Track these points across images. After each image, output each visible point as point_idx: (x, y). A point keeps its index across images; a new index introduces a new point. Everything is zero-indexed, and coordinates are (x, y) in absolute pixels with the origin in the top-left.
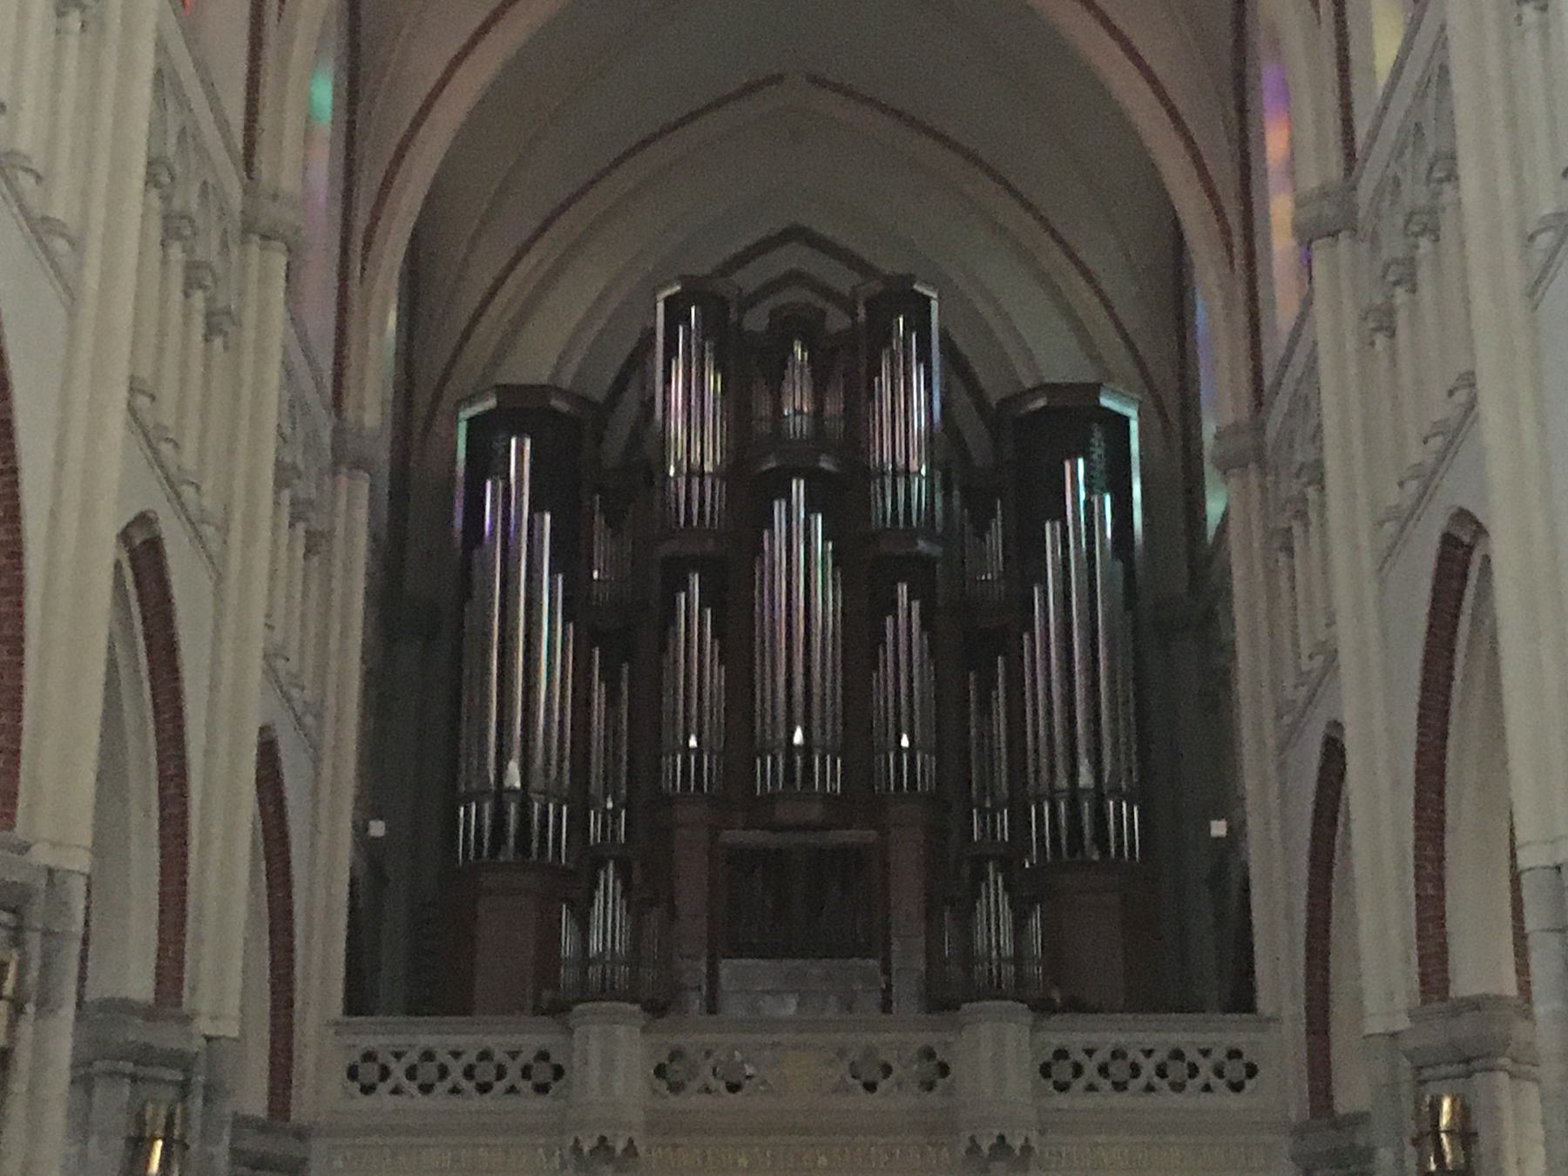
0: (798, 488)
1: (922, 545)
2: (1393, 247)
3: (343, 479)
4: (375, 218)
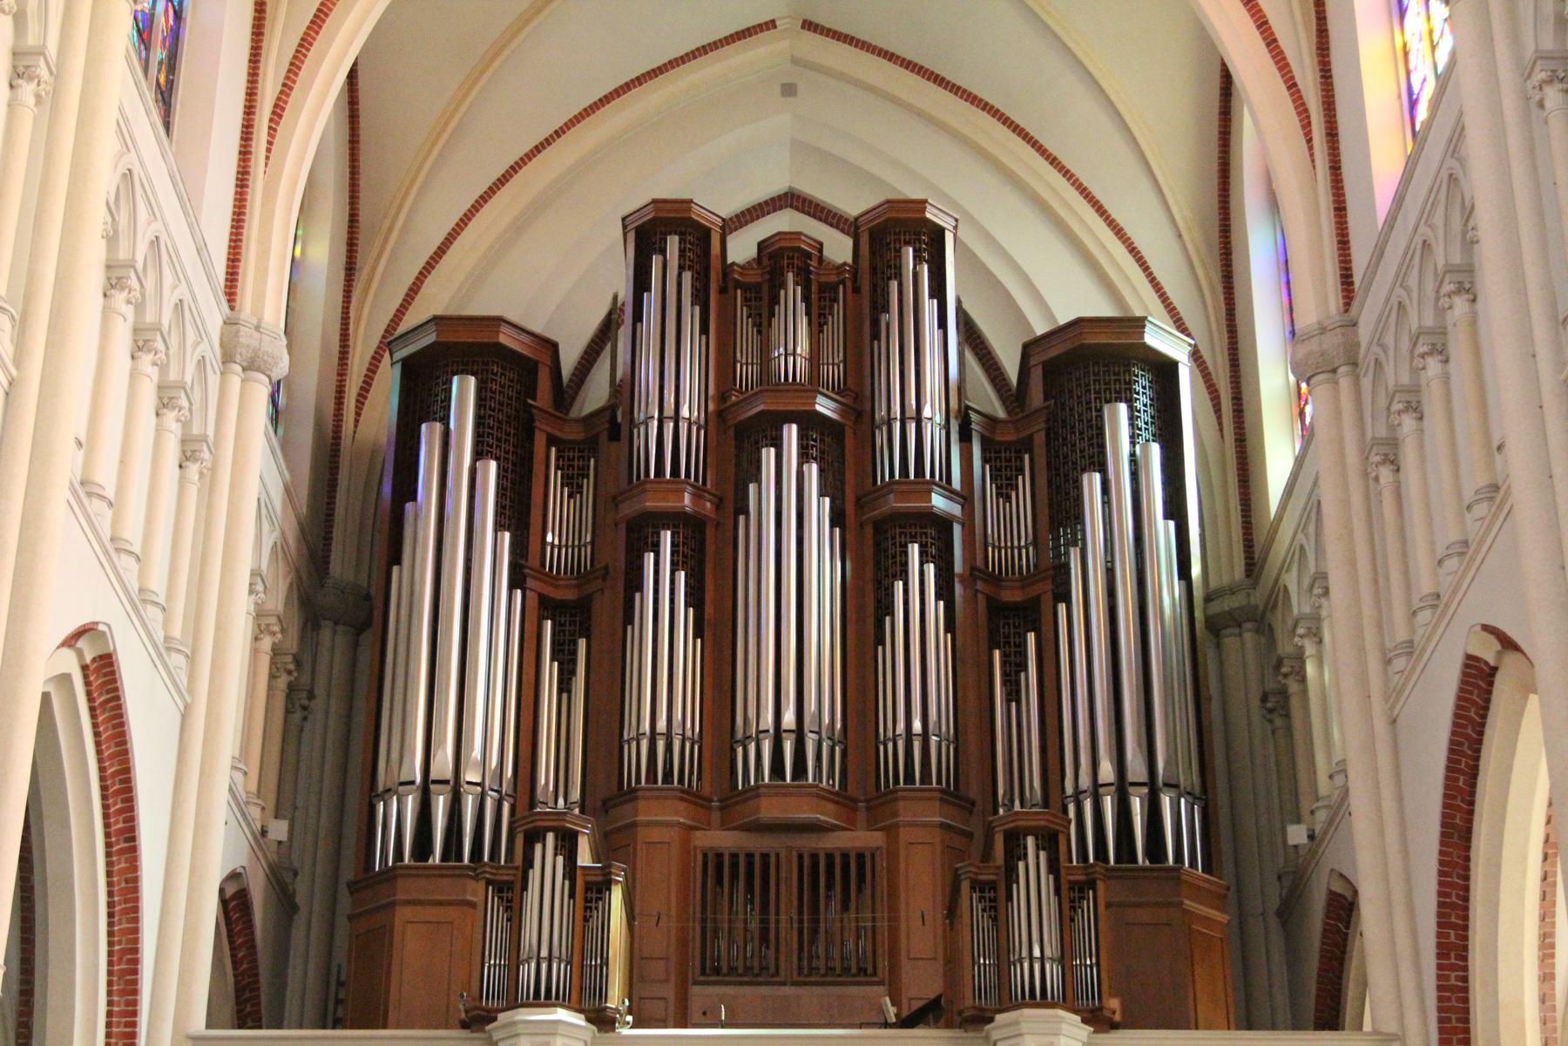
0: (791, 433)
1: (938, 501)
2: (1397, 374)
3: (235, 382)
4: (287, 88)
